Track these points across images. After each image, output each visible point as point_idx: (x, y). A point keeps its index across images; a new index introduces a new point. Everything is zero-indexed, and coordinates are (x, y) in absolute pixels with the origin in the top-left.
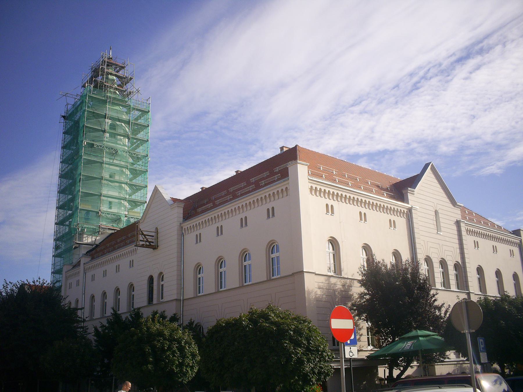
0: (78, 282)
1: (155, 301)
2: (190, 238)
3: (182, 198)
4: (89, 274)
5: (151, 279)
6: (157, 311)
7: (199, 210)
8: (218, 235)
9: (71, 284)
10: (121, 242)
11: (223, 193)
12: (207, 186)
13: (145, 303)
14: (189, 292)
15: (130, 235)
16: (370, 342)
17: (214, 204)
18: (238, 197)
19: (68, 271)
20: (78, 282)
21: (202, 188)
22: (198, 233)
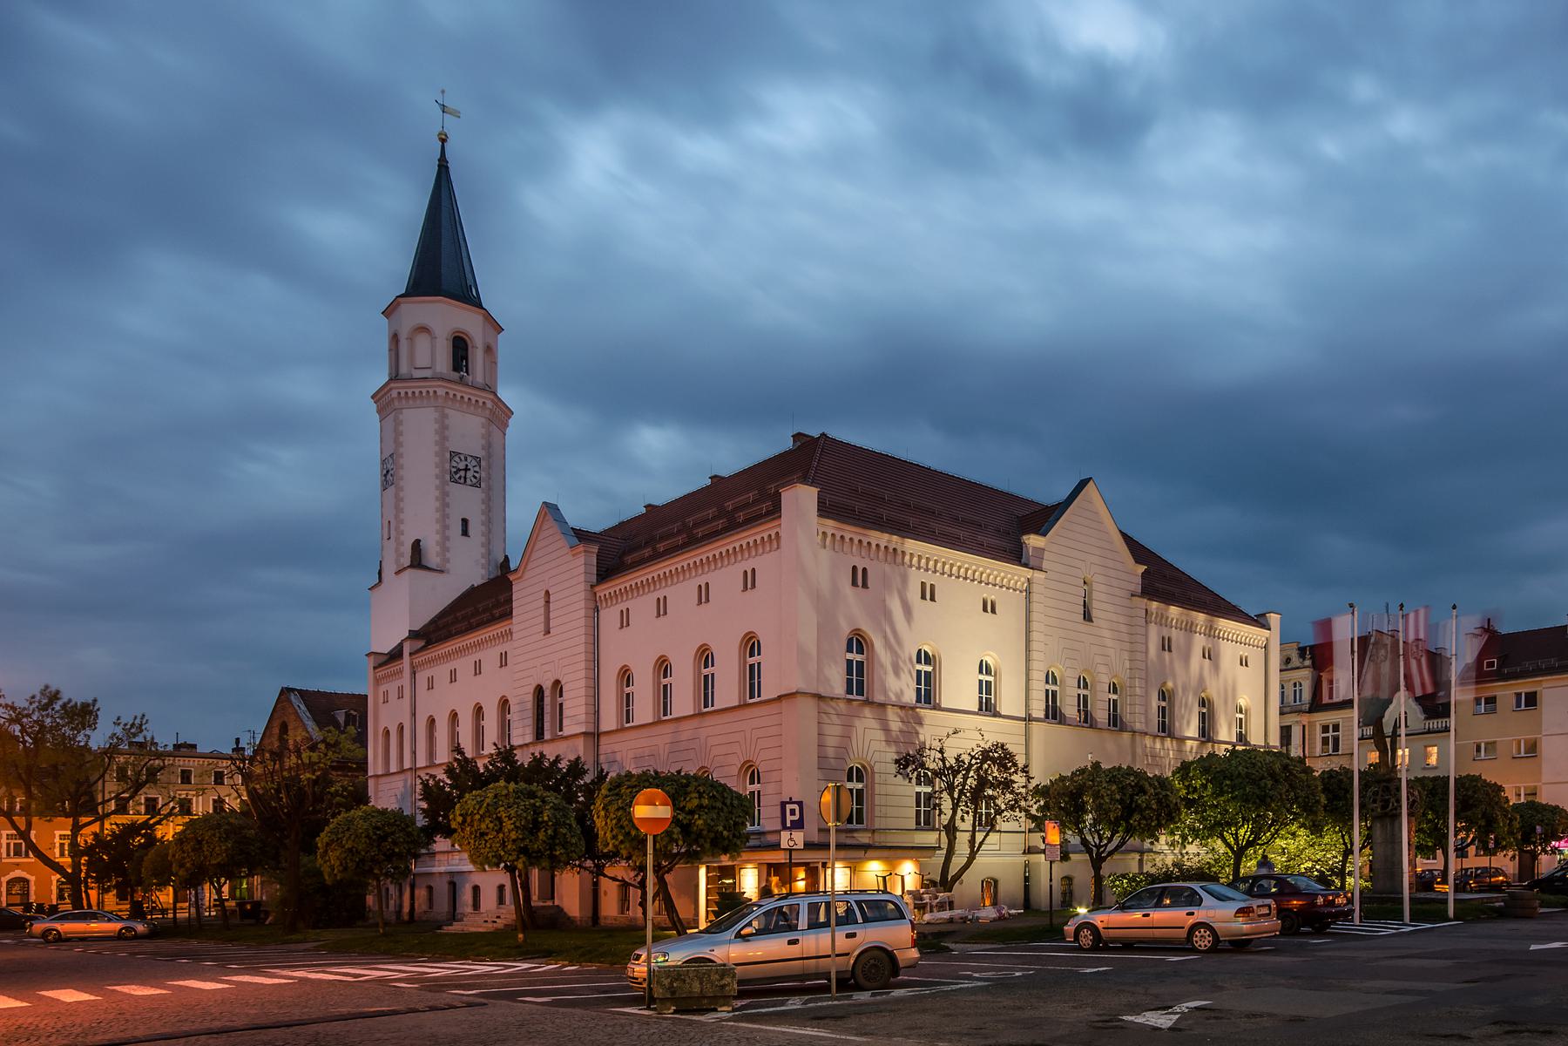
0: (401, 689)
1: (547, 736)
2: (609, 616)
3: (596, 527)
4: (422, 677)
5: (539, 691)
6: (58, 692)
7: (629, 559)
8: (700, 602)
9: (386, 694)
10: (484, 611)
11: (711, 512)
12: (659, 501)
13: (529, 739)
14: (609, 721)
15: (480, 606)
16: (1426, 907)
17: (654, 549)
18: (740, 525)
19: (417, 652)
20: (401, 689)
21: (797, 437)
22: (623, 606)
